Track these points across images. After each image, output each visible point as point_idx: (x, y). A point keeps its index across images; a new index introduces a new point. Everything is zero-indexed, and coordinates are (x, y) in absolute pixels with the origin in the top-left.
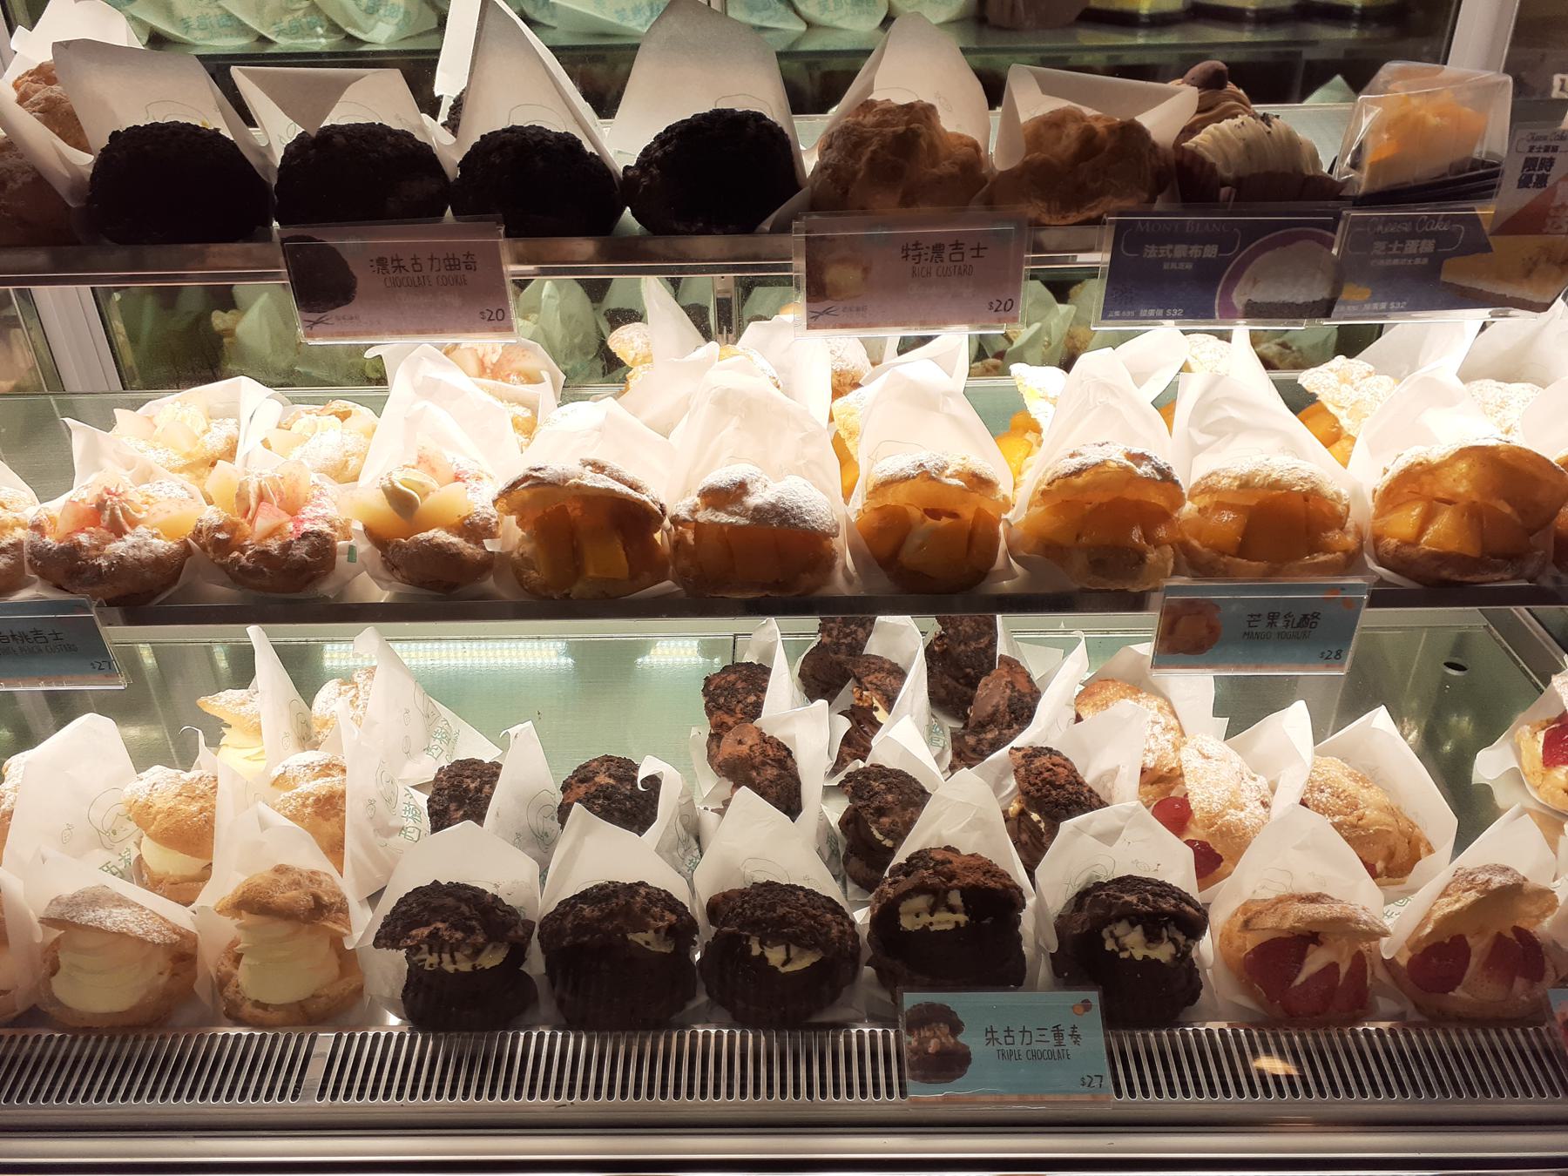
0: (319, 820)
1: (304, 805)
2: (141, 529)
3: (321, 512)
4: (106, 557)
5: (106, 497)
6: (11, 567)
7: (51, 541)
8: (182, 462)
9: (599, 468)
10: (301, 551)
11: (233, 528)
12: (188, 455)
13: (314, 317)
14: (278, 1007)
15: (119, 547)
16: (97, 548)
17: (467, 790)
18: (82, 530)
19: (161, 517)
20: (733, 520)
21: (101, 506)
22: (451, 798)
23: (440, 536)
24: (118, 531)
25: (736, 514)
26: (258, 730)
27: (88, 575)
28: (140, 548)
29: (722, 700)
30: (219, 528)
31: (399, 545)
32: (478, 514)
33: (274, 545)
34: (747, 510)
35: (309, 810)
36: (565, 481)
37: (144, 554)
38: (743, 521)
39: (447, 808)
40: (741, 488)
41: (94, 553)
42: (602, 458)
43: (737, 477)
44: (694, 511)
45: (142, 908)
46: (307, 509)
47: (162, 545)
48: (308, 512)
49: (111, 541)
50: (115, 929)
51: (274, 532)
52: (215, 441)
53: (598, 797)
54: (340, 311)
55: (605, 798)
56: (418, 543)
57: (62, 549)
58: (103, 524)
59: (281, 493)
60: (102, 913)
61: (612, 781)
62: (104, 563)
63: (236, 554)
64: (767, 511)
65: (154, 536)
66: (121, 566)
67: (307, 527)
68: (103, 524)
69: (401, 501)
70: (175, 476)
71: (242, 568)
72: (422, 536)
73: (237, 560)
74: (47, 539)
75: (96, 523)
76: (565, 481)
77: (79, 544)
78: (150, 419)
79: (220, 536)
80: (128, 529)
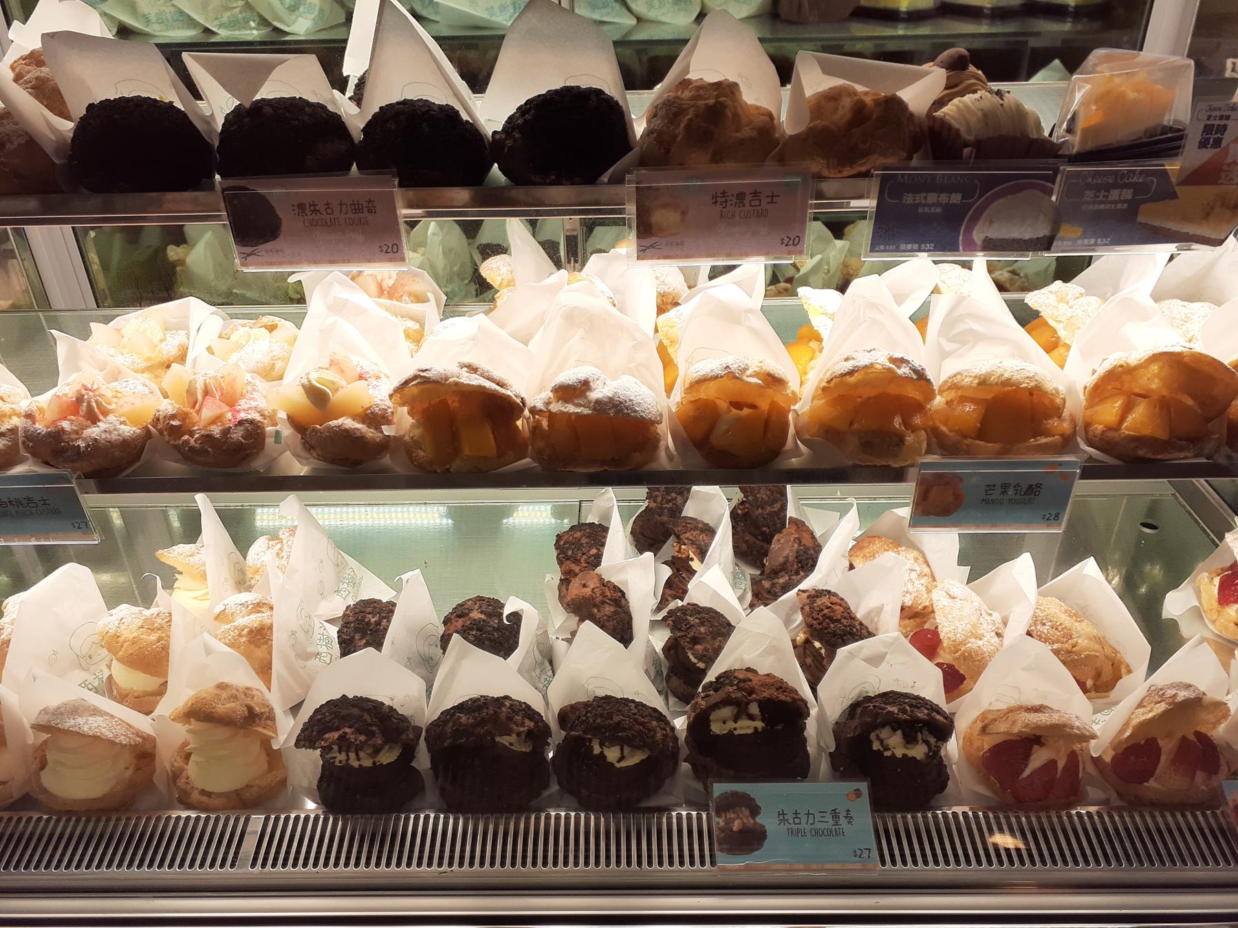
0: (252, 647)
1: (240, 635)
2: (111, 418)
3: (254, 404)
4: (84, 439)
5: (84, 392)
6: (9, 447)
7: (40, 427)
8: (144, 365)
9: (473, 369)
10: (237, 435)
11: (184, 416)
12: (149, 359)
13: (248, 250)
14: (220, 795)
15: (94, 432)
16: (76, 432)
17: (369, 623)
18: (65, 418)
19: (127, 408)
20: (578, 410)
21: (80, 399)
22: (356, 630)
23: (348, 423)
24: (93, 419)
25: (581, 405)
26: (204, 576)
27: (69, 454)
28: (110, 433)
29: (570, 553)
30: (173, 417)
31: (315, 430)
32: (377, 405)
33: (216, 430)
34: (590, 402)
35: (244, 639)
36: (446, 379)
37: (114, 437)
38: (586, 411)
39: (353, 638)
40: (585, 385)
41: (74, 436)
42: (475, 362)
43: (582, 377)
44: (548, 403)
45: (112, 716)
46: (242, 402)
47: (128, 430)
48: (243, 404)
49: (87, 427)
50: (91, 733)
51: (216, 420)
52: (170, 348)
53: (472, 629)
54: (268, 246)
55: (478, 630)
56: (330, 429)
57: (49, 434)
58: (82, 413)
59: (222, 389)
60: (80, 720)
61: (483, 617)
62: (82, 444)
63: (186, 437)
64: (606, 404)
65: (122, 423)
66: (95, 446)
67: (243, 415)
68: (82, 413)
69: (317, 396)
70: (139, 375)
71: (191, 448)
72: (333, 423)
73: (187, 442)
74: (37, 425)
75: (76, 413)
76: (446, 379)
77: (63, 429)
78: (118, 330)
79: (174, 423)
80: (101, 417)
